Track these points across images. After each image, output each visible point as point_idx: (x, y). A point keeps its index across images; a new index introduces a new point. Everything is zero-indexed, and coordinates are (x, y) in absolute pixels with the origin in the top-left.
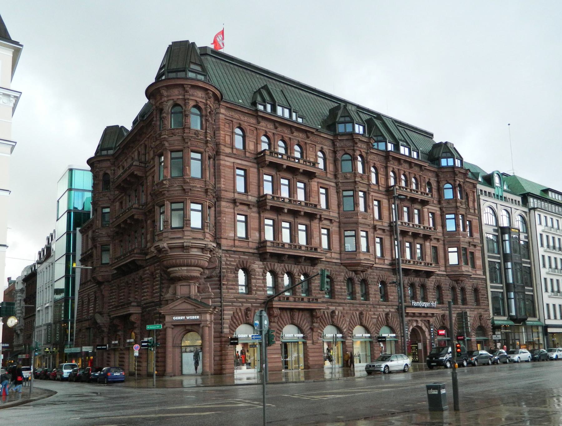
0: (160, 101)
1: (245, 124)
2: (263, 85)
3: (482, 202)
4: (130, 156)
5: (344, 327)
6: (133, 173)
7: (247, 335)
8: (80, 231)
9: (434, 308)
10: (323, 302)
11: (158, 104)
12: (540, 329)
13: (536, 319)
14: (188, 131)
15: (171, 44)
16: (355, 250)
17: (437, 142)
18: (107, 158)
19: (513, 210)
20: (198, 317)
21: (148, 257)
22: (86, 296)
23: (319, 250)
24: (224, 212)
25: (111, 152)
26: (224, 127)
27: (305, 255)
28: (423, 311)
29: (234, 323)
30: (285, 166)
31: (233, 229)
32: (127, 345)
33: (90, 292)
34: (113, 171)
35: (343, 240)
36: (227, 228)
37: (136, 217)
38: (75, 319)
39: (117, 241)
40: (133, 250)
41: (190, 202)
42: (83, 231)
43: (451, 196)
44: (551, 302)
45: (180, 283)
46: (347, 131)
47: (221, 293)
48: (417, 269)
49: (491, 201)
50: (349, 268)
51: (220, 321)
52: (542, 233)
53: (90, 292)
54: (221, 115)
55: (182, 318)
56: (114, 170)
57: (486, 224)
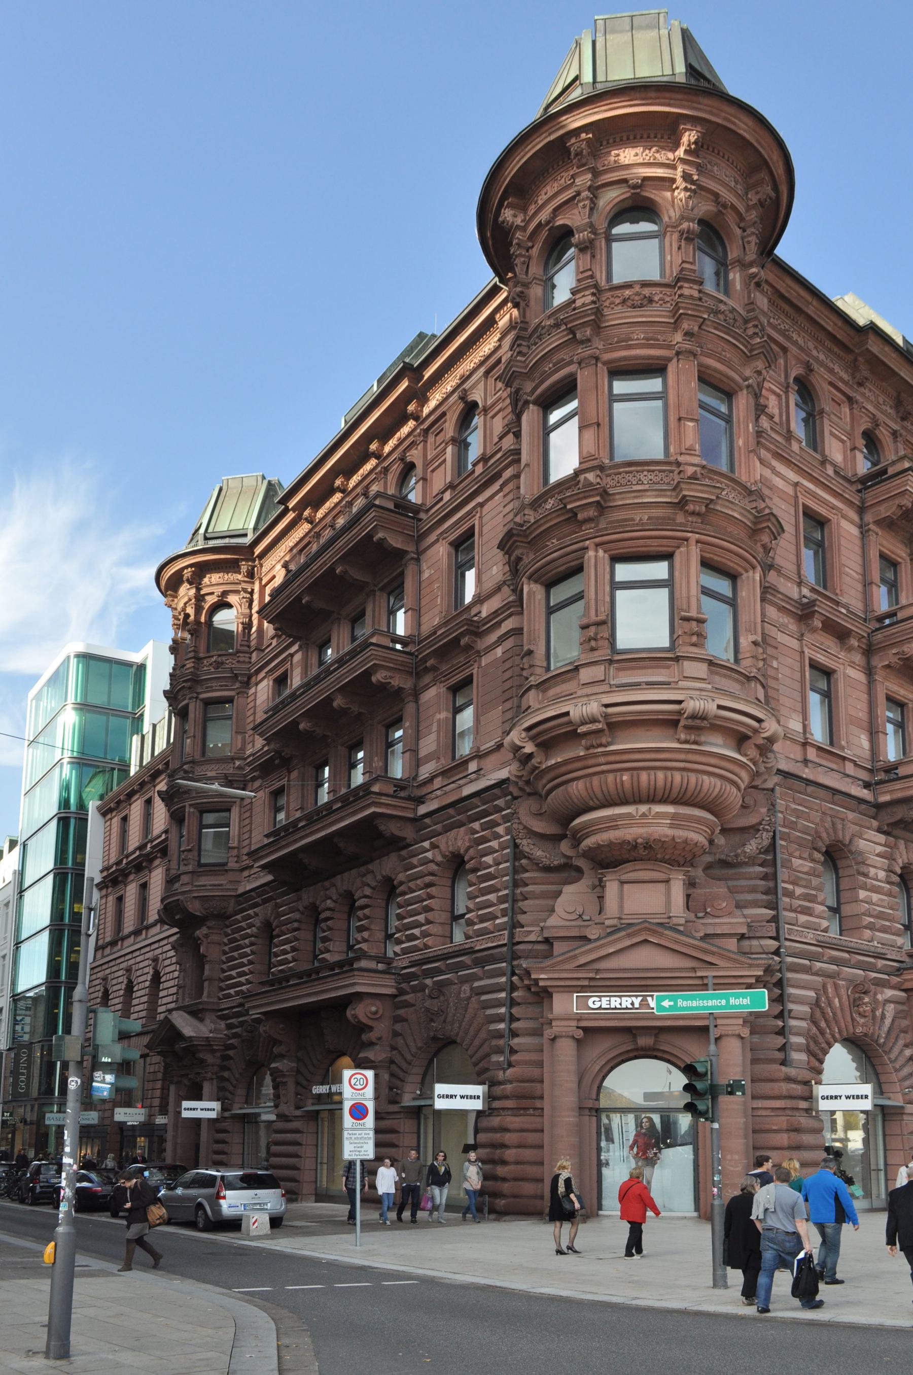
21: (422, 810)
22: (120, 973)
31: (799, 707)
37: (379, 677)
45: (630, 872)
47: (775, 919)
51: (781, 1024)
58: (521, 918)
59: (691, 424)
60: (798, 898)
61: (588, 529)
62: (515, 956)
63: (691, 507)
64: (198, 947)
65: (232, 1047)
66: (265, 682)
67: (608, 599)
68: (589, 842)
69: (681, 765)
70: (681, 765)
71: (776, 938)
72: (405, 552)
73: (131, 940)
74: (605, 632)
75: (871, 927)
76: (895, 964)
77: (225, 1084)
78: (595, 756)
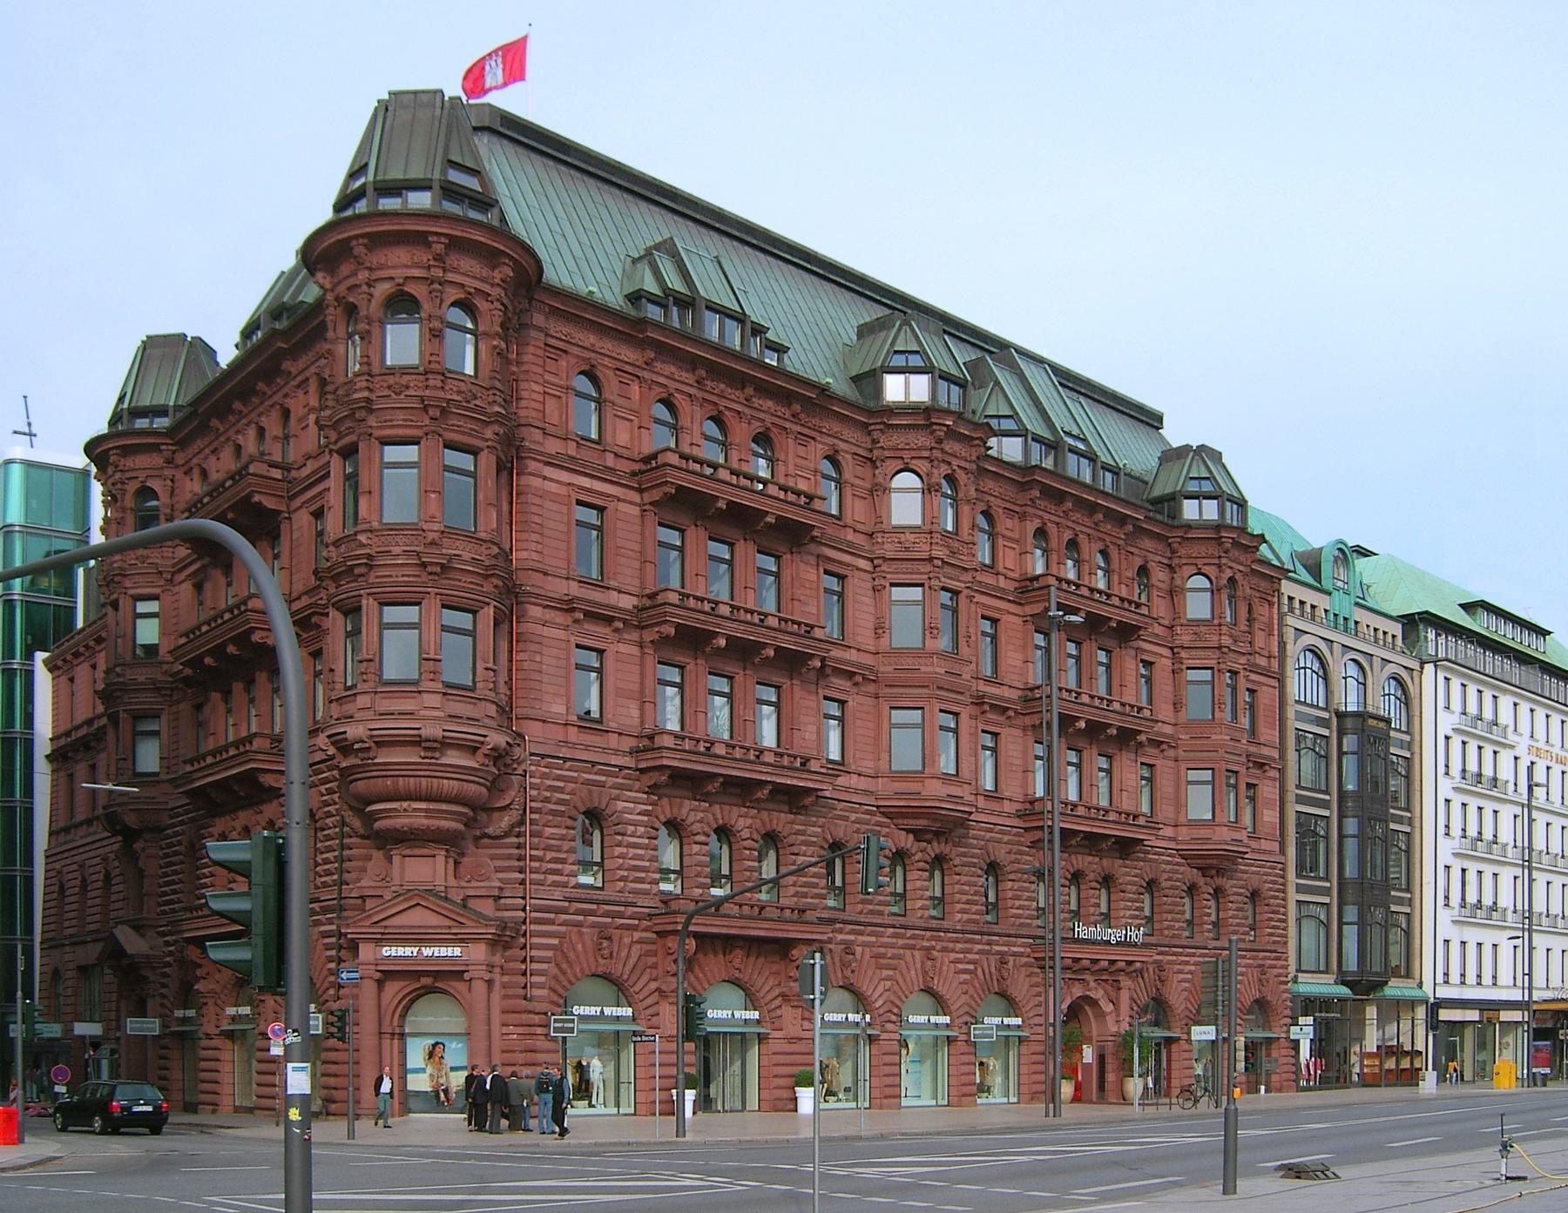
0: (351, 282)
1: (606, 361)
2: (659, 239)
3: (1290, 634)
4: (228, 439)
5: (877, 994)
6: (249, 496)
7: (599, 1009)
8: (46, 662)
9: (1135, 945)
10: (821, 921)
11: (342, 289)
12: (1421, 1012)
13: (1413, 983)
14: (439, 384)
15: (387, 97)
16: (920, 768)
17: (1175, 445)
18: (151, 440)
19: (1377, 662)
20: (457, 951)
23: (814, 766)
24: (538, 639)
25: (162, 423)
26: (540, 371)
27: (774, 779)
28: (1105, 956)
29: (564, 973)
30: (722, 505)
32: (225, 1021)
33: (85, 856)
34: (169, 483)
35: (885, 737)
36: (545, 688)
38: (38, 938)
39: (182, 706)
40: (249, 739)
41: (439, 604)
42: (60, 663)
43: (1205, 613)
44: (1446, 930)
46: (914, 398)
48: (1095, 830)
49: (1316, 632)
50: (900, 821)
52: (1450, 733)
53: (85, 856)
54: (533, 333)
55: (408, 951)
56: (172, 481)
57: (1298, 702)
58: (346, 876)
59: (433, 496)
60: (548, 862)
61: (361, 582)
62: (342, 909)
63: (429, 569)
64: (137, 859)
65: (168, 965)
66: (184, 585)
67: (376, 639)
68: (377, 825)
69: (427, 773)
70: (427, 773)
71: (524, 898)
72: (279, 512)
73: (83, 831)
74: (372, 667)
75: (623, 879)
76: (647, 910)
77: (165, 1001)
78: (369, 765)
